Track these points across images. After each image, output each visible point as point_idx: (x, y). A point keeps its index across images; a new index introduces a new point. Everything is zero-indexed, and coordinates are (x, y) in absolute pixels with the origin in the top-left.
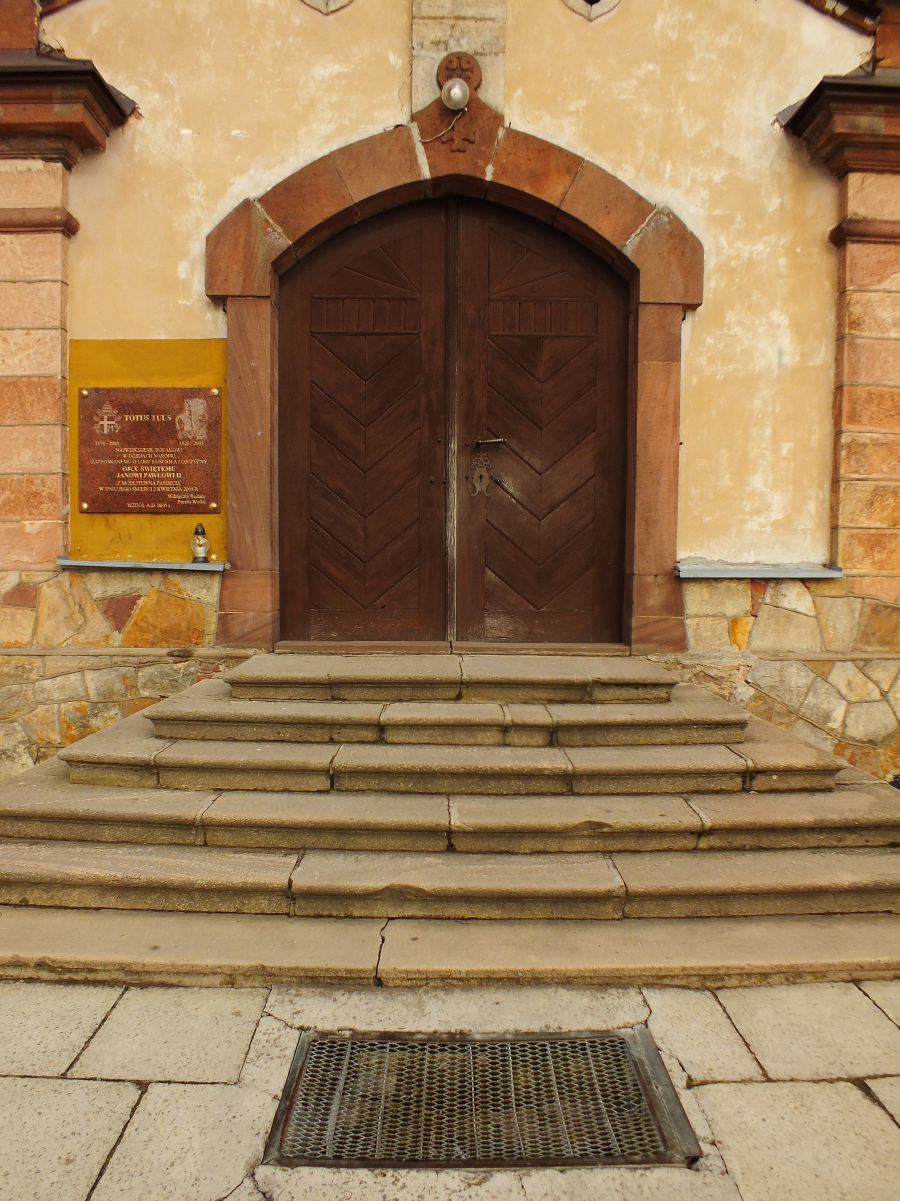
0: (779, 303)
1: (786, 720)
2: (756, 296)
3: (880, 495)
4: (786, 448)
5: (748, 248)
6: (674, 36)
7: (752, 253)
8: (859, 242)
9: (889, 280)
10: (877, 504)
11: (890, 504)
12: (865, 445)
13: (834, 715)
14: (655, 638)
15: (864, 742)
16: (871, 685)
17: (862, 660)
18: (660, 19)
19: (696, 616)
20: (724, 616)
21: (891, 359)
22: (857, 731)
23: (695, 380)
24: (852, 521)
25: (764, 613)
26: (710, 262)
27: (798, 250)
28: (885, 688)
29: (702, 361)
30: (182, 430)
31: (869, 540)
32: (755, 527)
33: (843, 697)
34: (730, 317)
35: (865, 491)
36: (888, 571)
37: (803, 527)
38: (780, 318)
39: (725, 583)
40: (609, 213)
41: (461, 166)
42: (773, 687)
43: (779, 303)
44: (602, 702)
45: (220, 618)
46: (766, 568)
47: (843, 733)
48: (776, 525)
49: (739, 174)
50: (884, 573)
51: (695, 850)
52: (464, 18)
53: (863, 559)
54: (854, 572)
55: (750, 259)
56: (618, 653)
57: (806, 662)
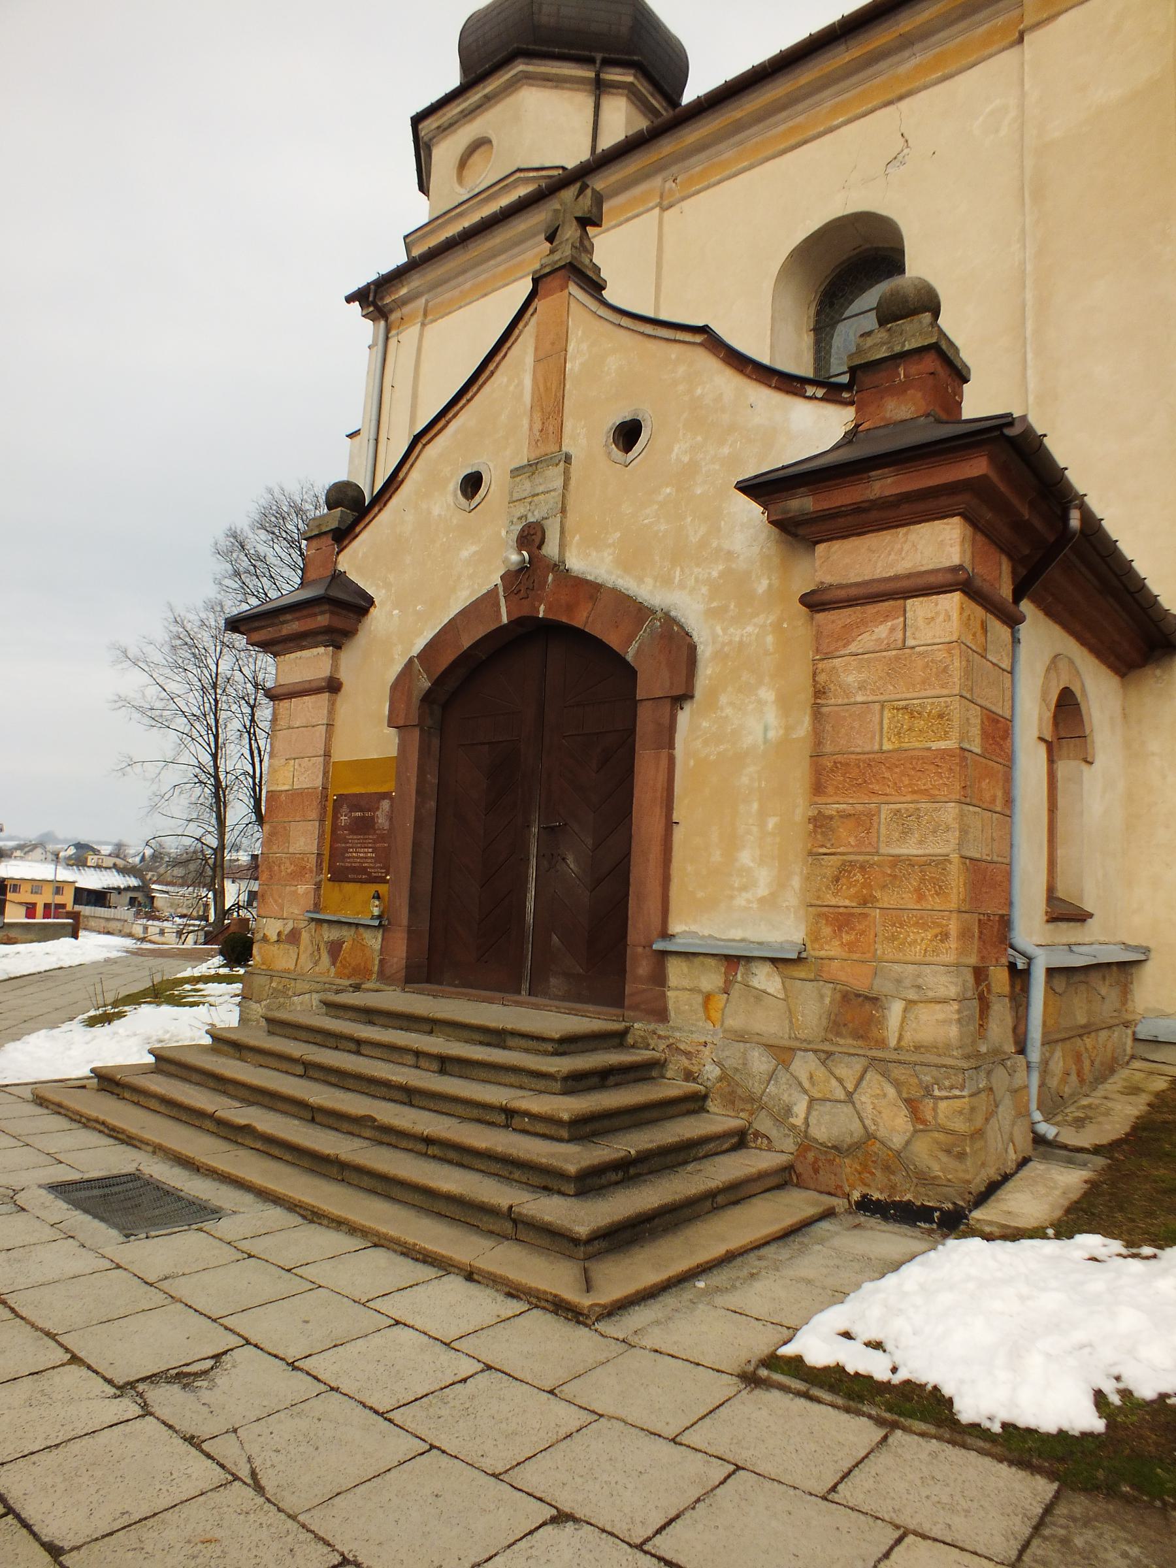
0: (767, 680)
1: (748, 1107)
2: (745, 676)
3: (846, 871)
4: (771, 823)
5: (739, 632)
6: (686, 459)
7: (742, 635)
8: (824, 610)
9: (855, 643)
10: (843, 881)
11: (858, 881)
12: (831, 818)
13: (795, 1109)
14: (643, 1007)
15: (828, 1147)
16: (834, 1082)
17: (823, 1051)
18: (676, 449)
19: (677, 989)
20: (700, 991)
21: (856, 724)
22: (821, 1132)
23: (692, 763)
24: (818, 898)
25: (736, 990)
26: (705, 652)
27: (785, 625)
28: (850, 1088)
29: (698, 744)
31: (837, 920)
32: (743, 903)
33: (805, 1092)
34: (723, 699)
35: (832, 866)
36: (858, 955)
37: (787, 904)
38: (767, 694)
39: (701, 958)
40: (617, 627)
41: (525, 611)
42: (737, 1070)
43: (767, 680)
44: (510, 1049)
45: (381, 961)
46: (752, 945)
47: (806, 1132)
48: (762, 901)
49: (734, 566)
50: (855, 956)
51: (425, 1155)
52: (538, 494)
53: (831, 939)
54: (822, 953)
55: (741, 643)
56: (615, 1018)
57: (769, 1046)
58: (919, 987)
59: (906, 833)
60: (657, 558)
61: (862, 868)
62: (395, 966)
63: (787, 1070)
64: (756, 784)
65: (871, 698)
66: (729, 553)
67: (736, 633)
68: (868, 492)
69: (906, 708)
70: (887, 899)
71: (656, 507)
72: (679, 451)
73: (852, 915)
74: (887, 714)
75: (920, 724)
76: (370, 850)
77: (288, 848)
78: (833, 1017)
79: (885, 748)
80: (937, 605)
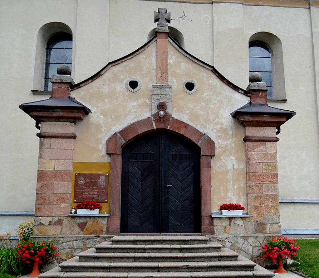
2: (227, 152)
4: (236, 187)
10: (256, 199)
12: (253, 186)
19: (216, 226)
25: (232, 225)
26: (217, 145)
30: (99, 183)
34: (222, 158)
41: (162, 126)
43: (233, 154)
49: (223, 127)
50: (259, 215)
52: (163, 95)
54: (252, 215)
55: (226, 145)
58: (273, 221)
59: (269, 190)
60: (201, 120)
61: (260, 197)
62: (114, 229)
63: (247, 241)
64: (232, 178)
65: (260, 161)
66: (221, 123)
67: (225, 143)
68: (263, 119)
69: (267, 164)
70: (265, 203)
71: (200, 107)
72: (206, 95)
73: (259, 207)
74: (263, 165)
75: (270, 168)
76: (96, 192)
77: (53, 191)
78: (255, 228)
79: (263, 172)
80: (272, 144)
